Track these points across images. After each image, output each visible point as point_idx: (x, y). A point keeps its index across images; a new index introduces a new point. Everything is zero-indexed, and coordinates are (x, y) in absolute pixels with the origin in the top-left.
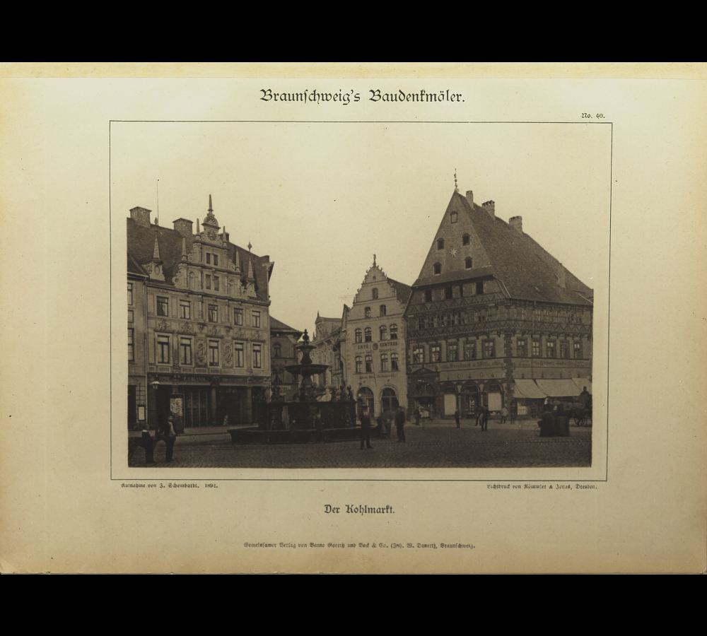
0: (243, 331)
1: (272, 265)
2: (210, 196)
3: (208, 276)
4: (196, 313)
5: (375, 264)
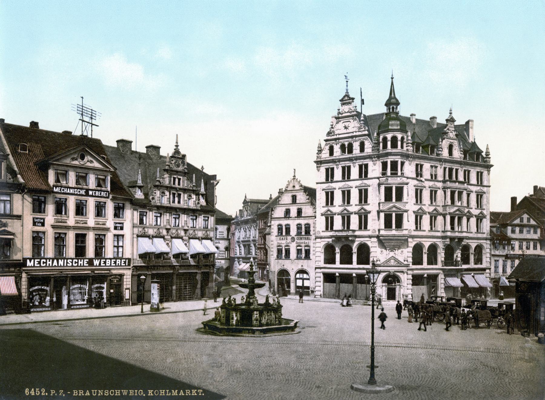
0: (208, 232)
1: (218, 182)
2: (177, 135)
3: (174, 194)
4: (183, 222)
5: (294, 176)
